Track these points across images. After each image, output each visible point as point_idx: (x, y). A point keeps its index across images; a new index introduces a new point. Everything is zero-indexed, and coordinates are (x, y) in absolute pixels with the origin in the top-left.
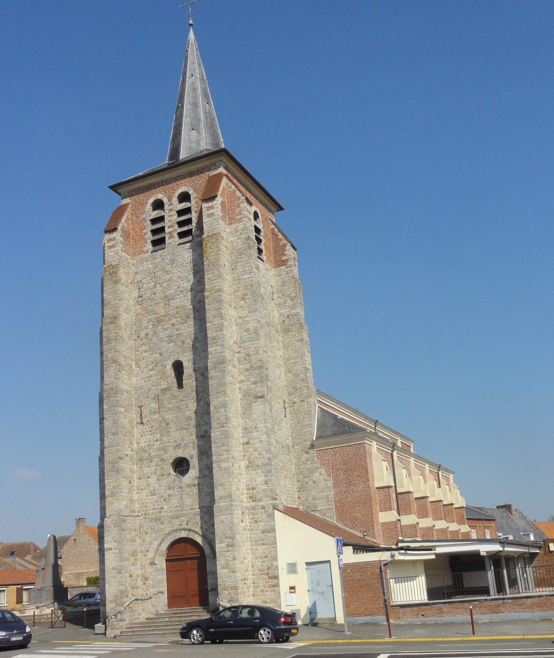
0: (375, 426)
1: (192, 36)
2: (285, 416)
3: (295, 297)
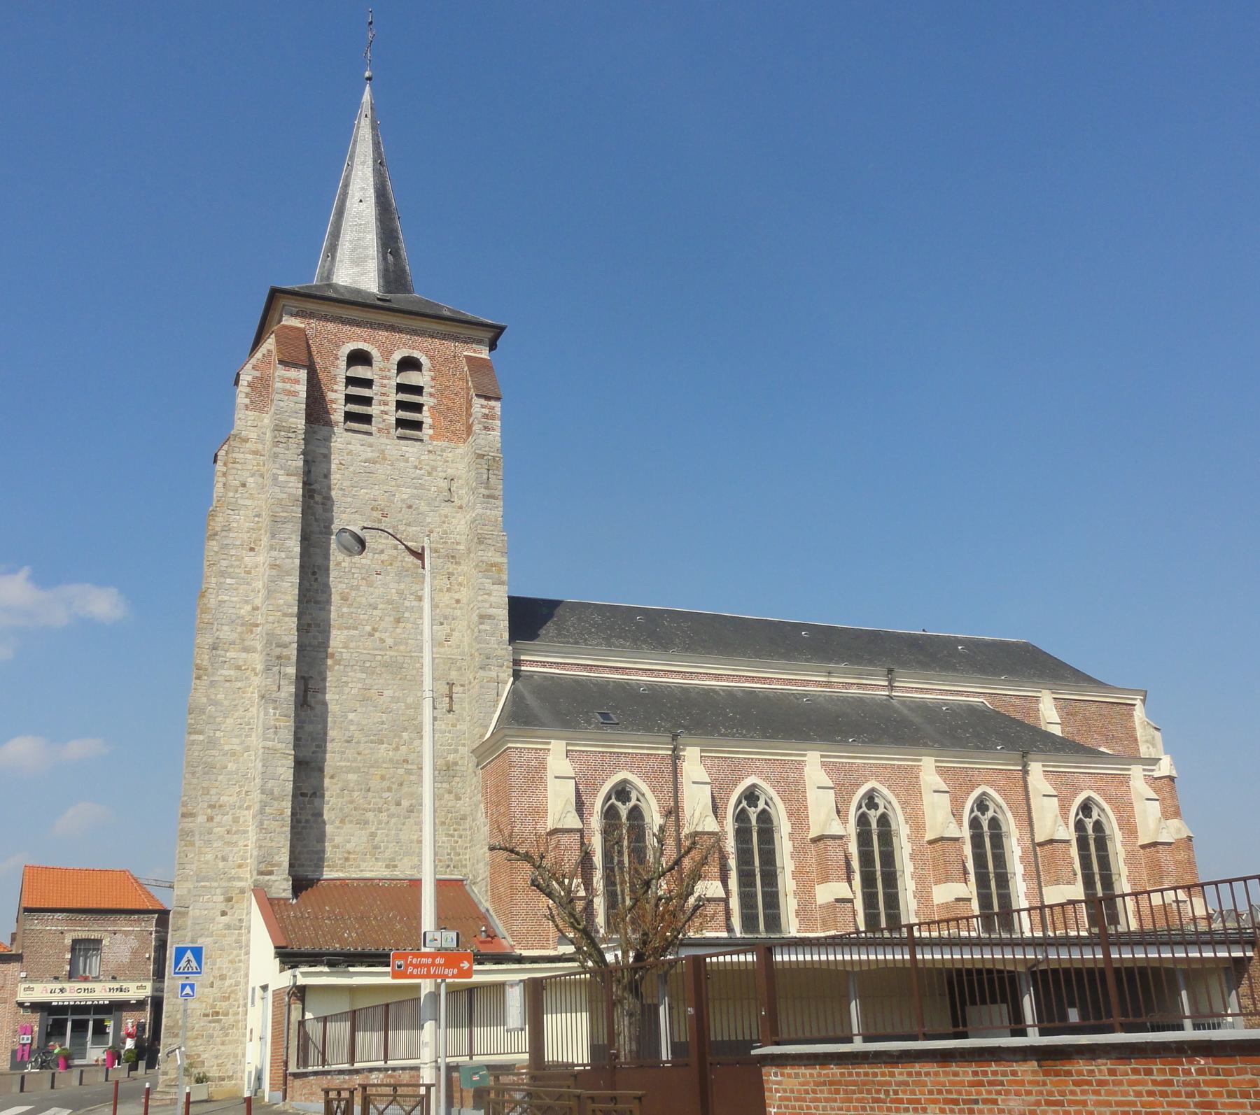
0: (890, 681)
1: (367, 97)
2: (450, 711)
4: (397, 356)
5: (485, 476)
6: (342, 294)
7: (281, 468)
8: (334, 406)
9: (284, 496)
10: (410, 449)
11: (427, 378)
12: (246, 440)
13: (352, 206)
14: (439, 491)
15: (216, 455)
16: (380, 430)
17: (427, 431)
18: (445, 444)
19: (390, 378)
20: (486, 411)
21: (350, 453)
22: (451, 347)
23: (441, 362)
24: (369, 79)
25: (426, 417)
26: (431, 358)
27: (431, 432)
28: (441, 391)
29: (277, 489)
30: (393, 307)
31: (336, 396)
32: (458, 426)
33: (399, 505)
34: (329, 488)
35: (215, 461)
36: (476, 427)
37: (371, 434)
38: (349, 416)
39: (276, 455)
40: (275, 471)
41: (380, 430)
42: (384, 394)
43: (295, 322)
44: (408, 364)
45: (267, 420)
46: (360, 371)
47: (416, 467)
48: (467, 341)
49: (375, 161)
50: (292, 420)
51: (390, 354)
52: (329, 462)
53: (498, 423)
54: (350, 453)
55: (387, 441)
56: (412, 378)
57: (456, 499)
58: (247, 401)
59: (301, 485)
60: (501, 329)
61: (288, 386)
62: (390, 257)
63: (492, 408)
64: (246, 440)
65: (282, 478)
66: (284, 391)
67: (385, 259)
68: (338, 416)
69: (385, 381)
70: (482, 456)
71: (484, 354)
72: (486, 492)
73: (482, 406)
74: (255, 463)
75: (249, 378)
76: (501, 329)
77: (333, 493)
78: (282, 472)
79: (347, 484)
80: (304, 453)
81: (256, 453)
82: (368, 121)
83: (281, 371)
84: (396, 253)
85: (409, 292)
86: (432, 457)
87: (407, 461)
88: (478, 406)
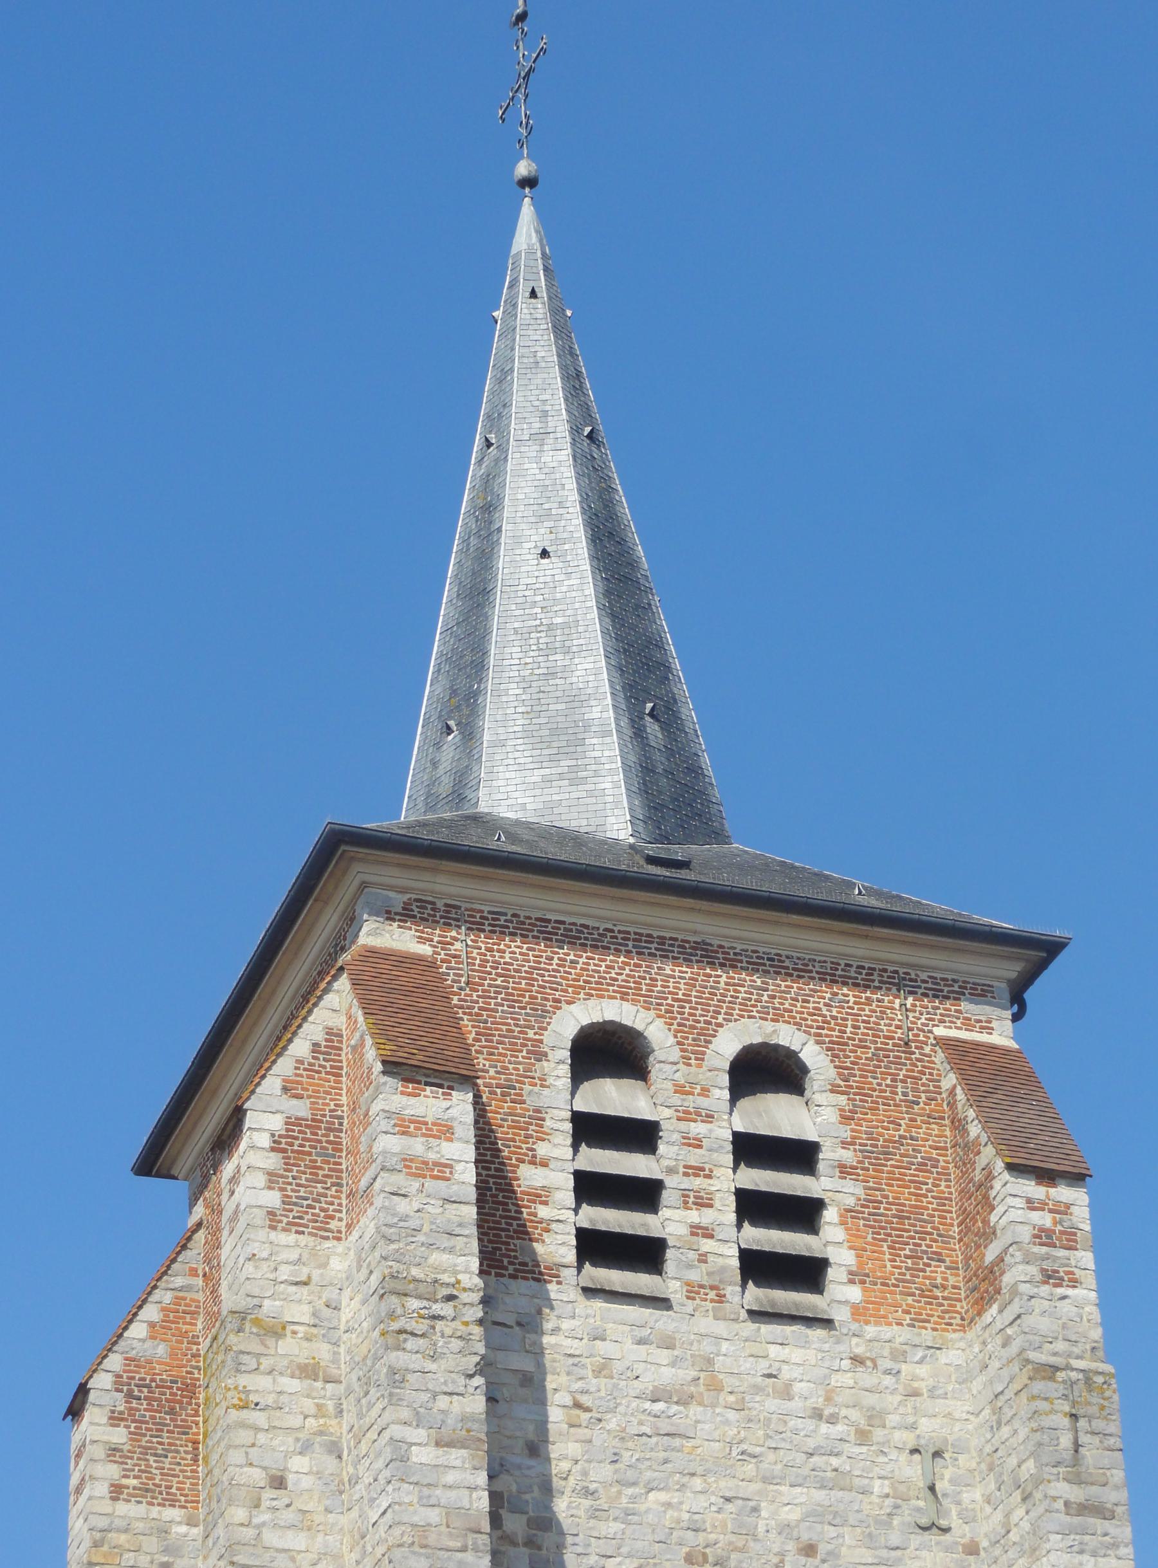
1: (526, 235)
3: (1038, 1481)
4: (728, 1044)
5: (1066, 1441)
6: (512, 838)
7: (418, 1421)
8: (543, 1212)
9: (434, 1516)
10: (795, 1353)
11: (829, 1115)
12: (276, 1330)
13: (515, 564)
14: (899, 1496)
15: (83, 1391)
16: (693, 1291)
17: (841, 1292)
18: (902, 1335)
19: (709, 1118)
20: (1045, 1219)
21: (602, 1369)
22: (898, 1012)
23: (869, 1071)
24: (529, 182)
25: (832, 1240)
26: (835, 1049)
27: (854, 1293)
28: (873, 1159)
29: (409, 1495)
30: (674, 884)
31: (549, 1174)
32: (938, 1272)
33: (775, 1543)
34: (547, 1489)
35: (75, 1411)
36: (1017, 1274)
37: (661, 1303)
38: (594, 1246)
39: (397, 1377)
40: (396, 1431)
41: (693, 1291)
42: (697, 1171)
43: (401, 939)
44: (764, 1071)
45: (339, 1259)
46: (612, 1097)
47: (817, 1415)
48: (943, 990)
49: (575, 431)
50: (436, 1258)
51: (706, 1036)
52: (541, 1401)
53: (1085, 1258)
54: (602, 1369)
55: (721, 1328)
56: (775, 1114)
57: (953, 1519)
58: (273, 1199)
59: (482, 1478)
60: (1052, 948)
61: (417, 1146)
62: (652, 728)
63: (1061, 1210)
64: (276, 1330)
65: (423, 1455)
66: (407, 1161)
67: (639, 733)
68: (557, 1247)
69: (698, 1129)
70: (1049, 1371)
71: (1001, 1033)
72: (1075, 1494)
73: (1032, 1205)
74: (309, 1405)
75: (276, 1123)
76: (1052, 948)
77: (561, 1506)
78: (420, 1435)
79: (602, 1473)
80: (485, 1367)
81: (309, 1371)
82: (540, 308)
83: (392, 1097)
84: (667, 714)
85: (719, 836)
86: (867, 1378)
87: (786, 1393)
88: (1016, 1204)
